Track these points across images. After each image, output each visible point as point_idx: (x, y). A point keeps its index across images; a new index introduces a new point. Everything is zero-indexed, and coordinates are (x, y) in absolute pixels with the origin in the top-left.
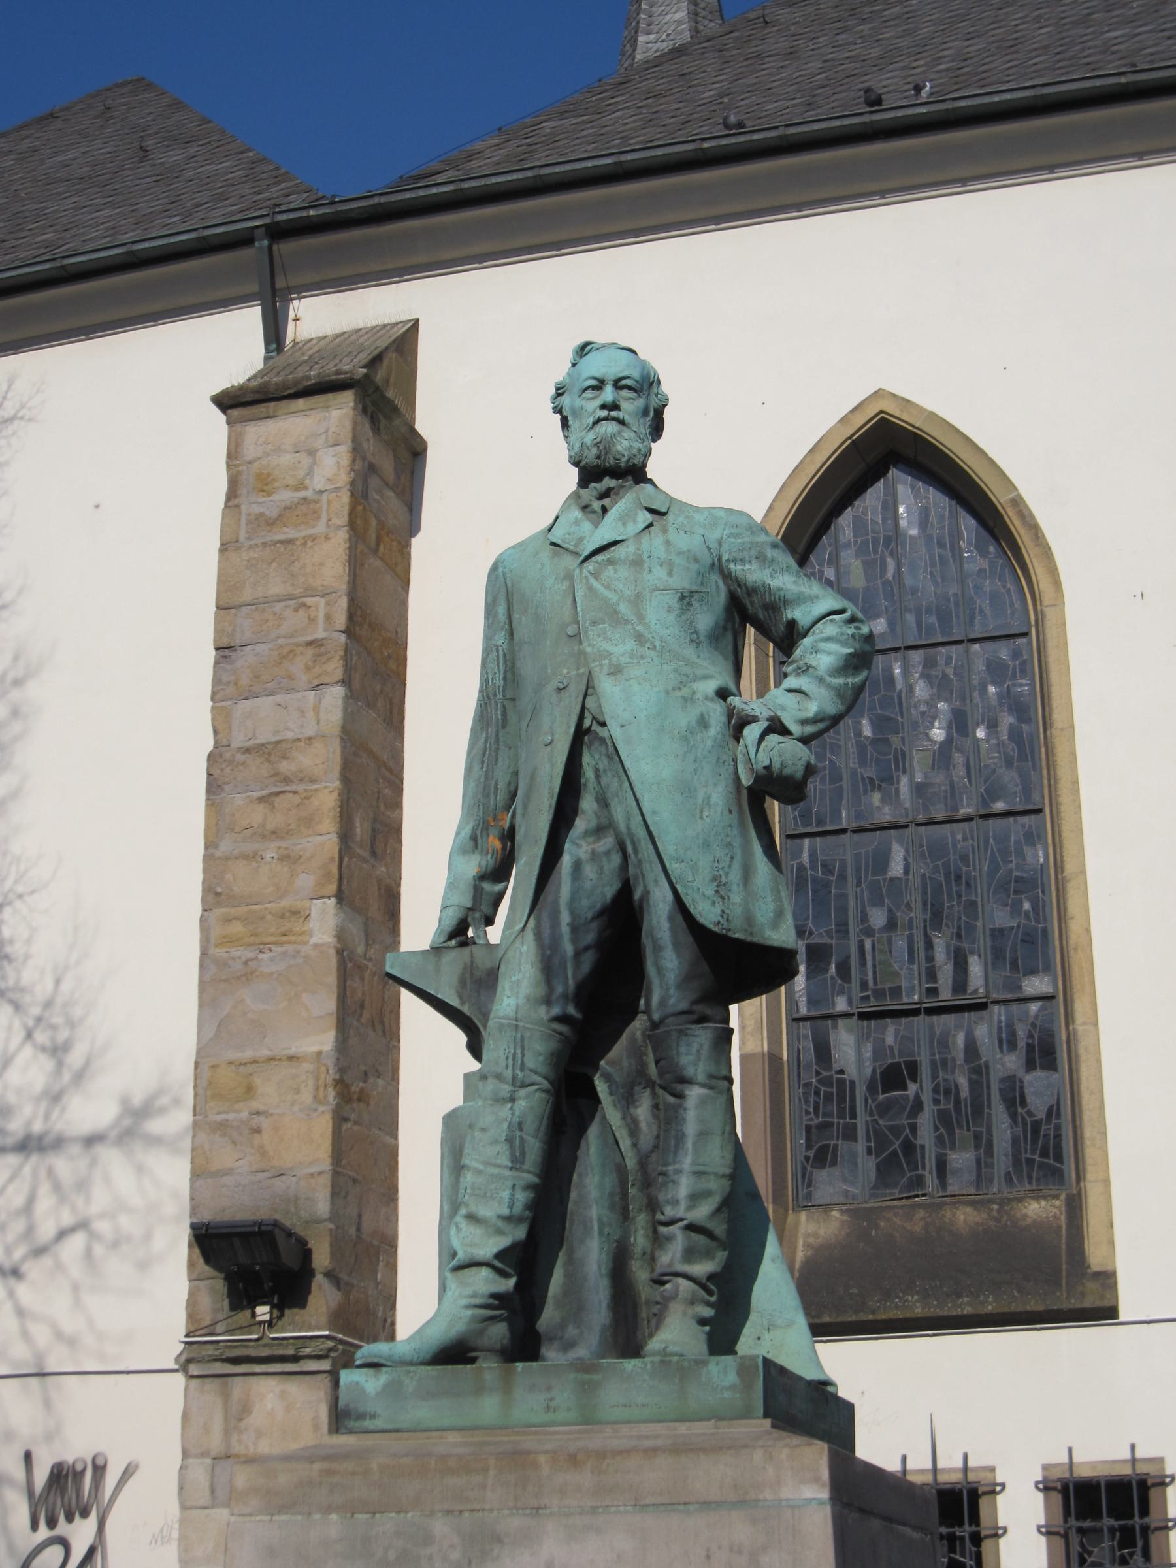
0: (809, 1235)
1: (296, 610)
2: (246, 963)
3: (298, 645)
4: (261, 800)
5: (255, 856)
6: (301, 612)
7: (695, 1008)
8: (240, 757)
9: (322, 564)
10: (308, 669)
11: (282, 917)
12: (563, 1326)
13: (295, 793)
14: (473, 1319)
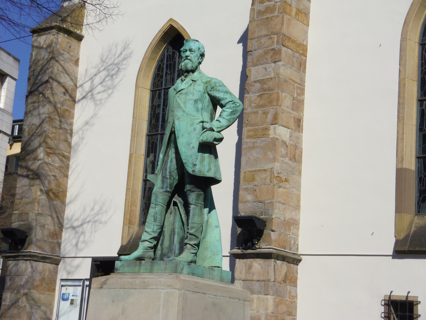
0: (416, 223)
1: (269, 39)
2: (253, 143)
3: (269, 50)
4: (258, 96)
5: (256, 113)
6: (270, 40)
7: (192, 189)
8: (253, 84)
9: (276, 25)
10: (271, 57)
11: (263, 130)
12: (168, 253)
13: (267, 94)
14: (143, 251)
